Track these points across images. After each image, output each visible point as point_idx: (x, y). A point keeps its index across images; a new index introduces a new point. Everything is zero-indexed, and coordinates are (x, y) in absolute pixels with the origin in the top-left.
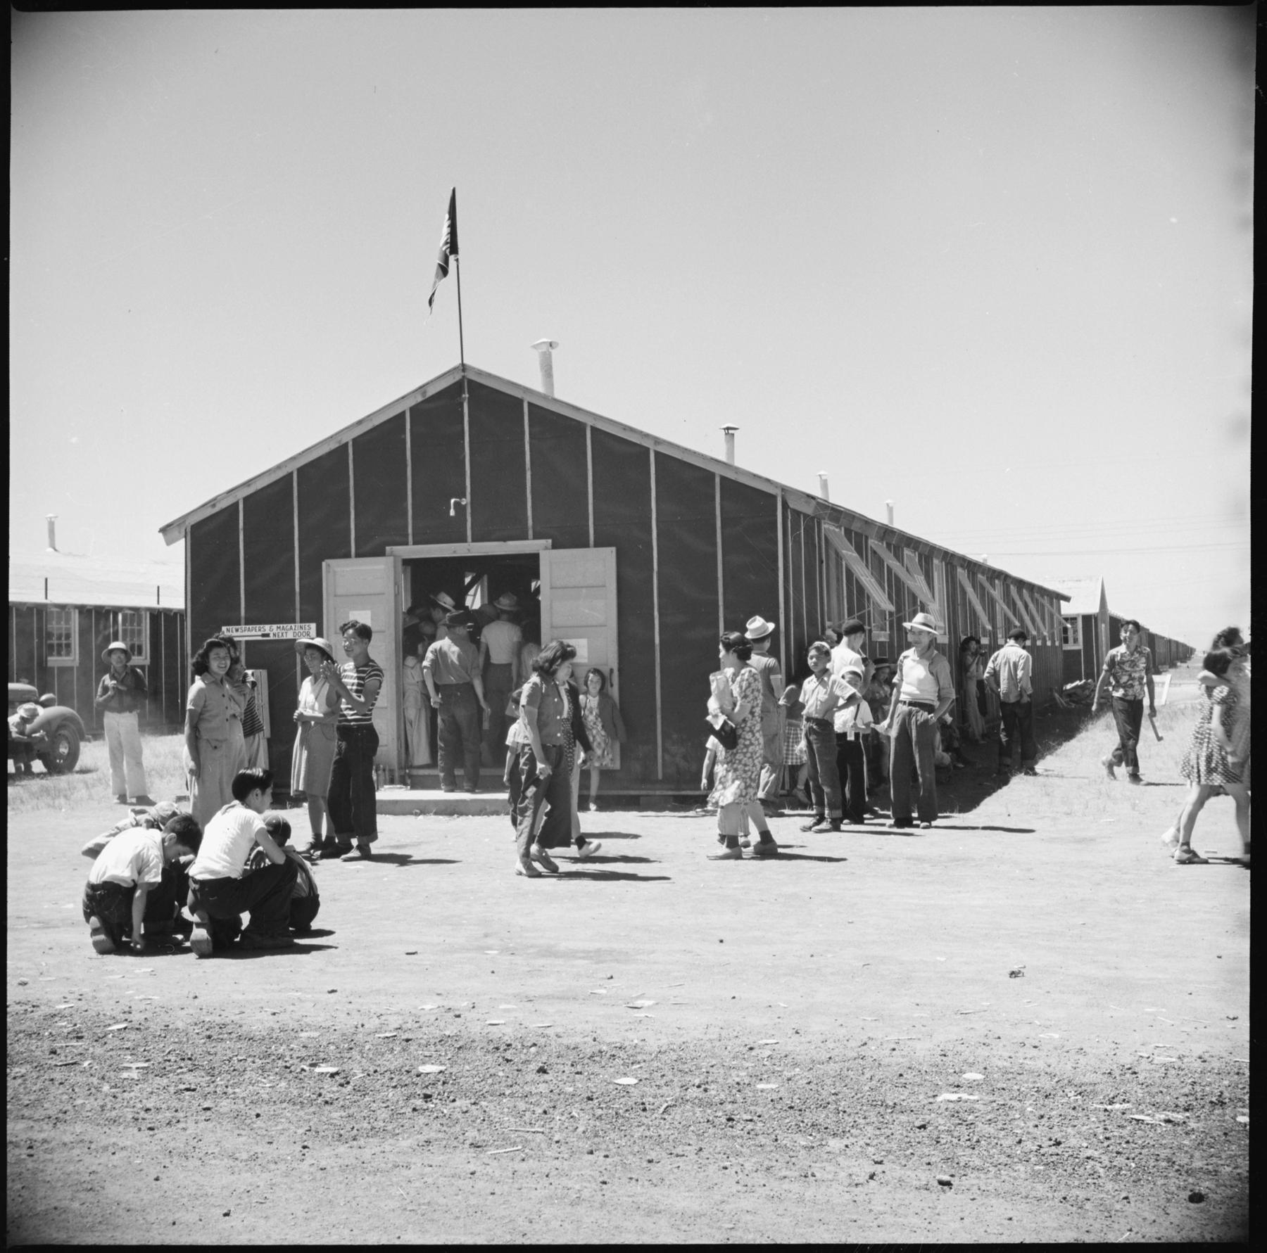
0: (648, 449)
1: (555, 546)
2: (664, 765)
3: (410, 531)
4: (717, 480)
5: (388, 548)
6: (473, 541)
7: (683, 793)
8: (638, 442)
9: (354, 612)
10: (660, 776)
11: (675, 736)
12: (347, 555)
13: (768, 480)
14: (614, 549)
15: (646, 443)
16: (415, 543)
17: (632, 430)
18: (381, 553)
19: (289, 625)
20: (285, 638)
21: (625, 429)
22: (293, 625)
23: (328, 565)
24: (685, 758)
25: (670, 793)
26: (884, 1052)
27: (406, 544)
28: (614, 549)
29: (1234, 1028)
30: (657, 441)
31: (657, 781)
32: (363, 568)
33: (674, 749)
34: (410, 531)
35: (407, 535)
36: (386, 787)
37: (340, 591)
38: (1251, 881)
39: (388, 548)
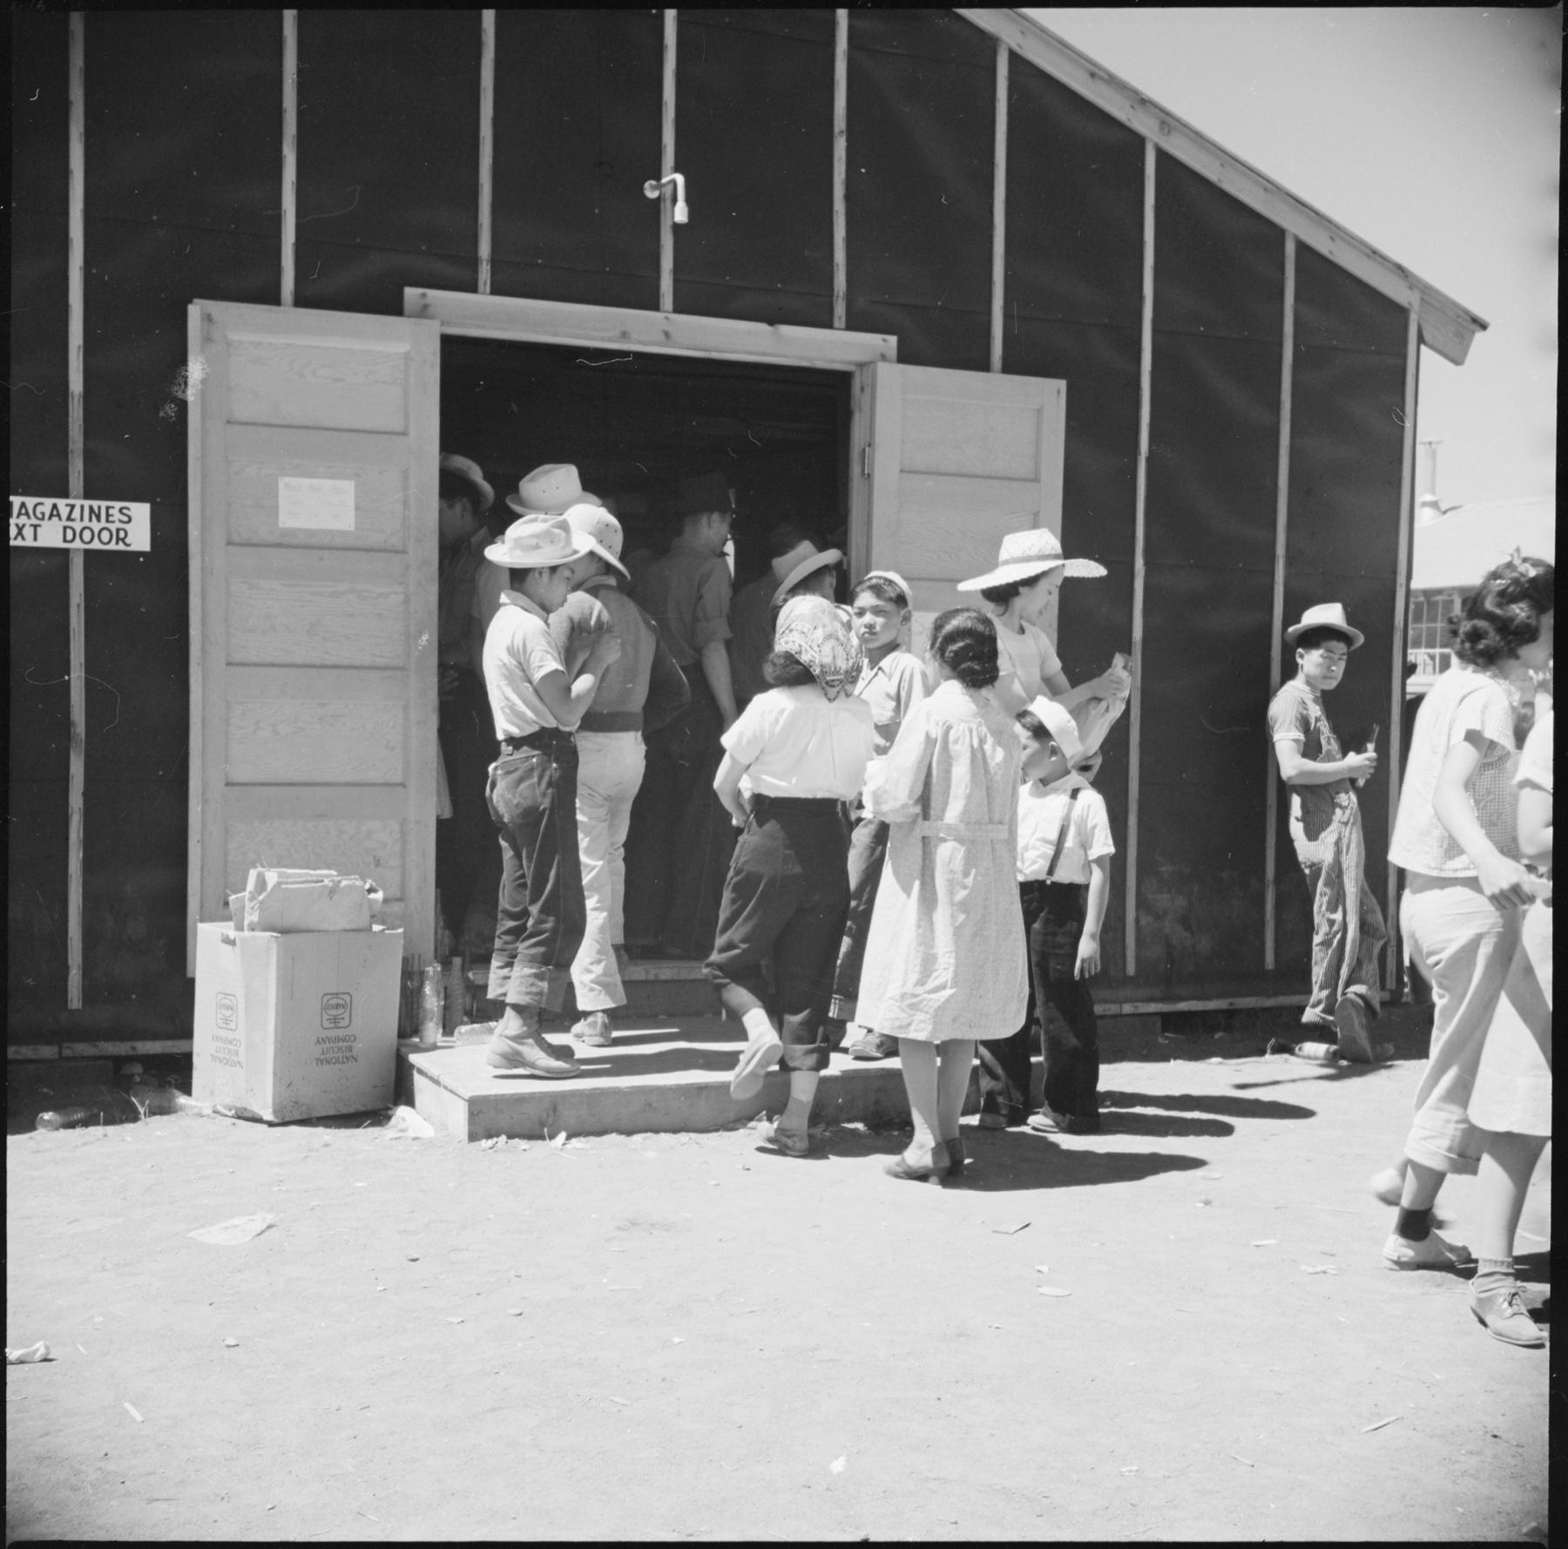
0: (1140, 141)
1: (906, 356)
2: (1140, 941)
3: (485, 249)
4: (1290, 248)
5: (411, 293)
6: (679, 308)
7: (1183, 1006)
8: (787, 330)
9: (295, 481)
10: (1131, 969)
11: (1165, 869)
12: (271, 296)
13: (1400, 269)
14: (1062, 384)
15: (1142, 124)
16: (496, 291)
17: (1112, 81)
18: (393, 307)
19: (48, 503)
20: (29, 542)
21: (1093, 75)
22: (62, 503)
23: (208, 318)
24: (1184, 921)
25: (1153, 1007)
26: (1494, 1502)
27: (472, 288)
28: (1062, 384)
29: (718, 1185)
30: (1168, 121)
31: (1127, 981)
32: (335, 342)
33: (1163, 900)
34: (485, 249)
35: (474, 262)
36: (463, 1029)
37: (242, 411)
38: (1553, 1094)
39: (411, 293)
